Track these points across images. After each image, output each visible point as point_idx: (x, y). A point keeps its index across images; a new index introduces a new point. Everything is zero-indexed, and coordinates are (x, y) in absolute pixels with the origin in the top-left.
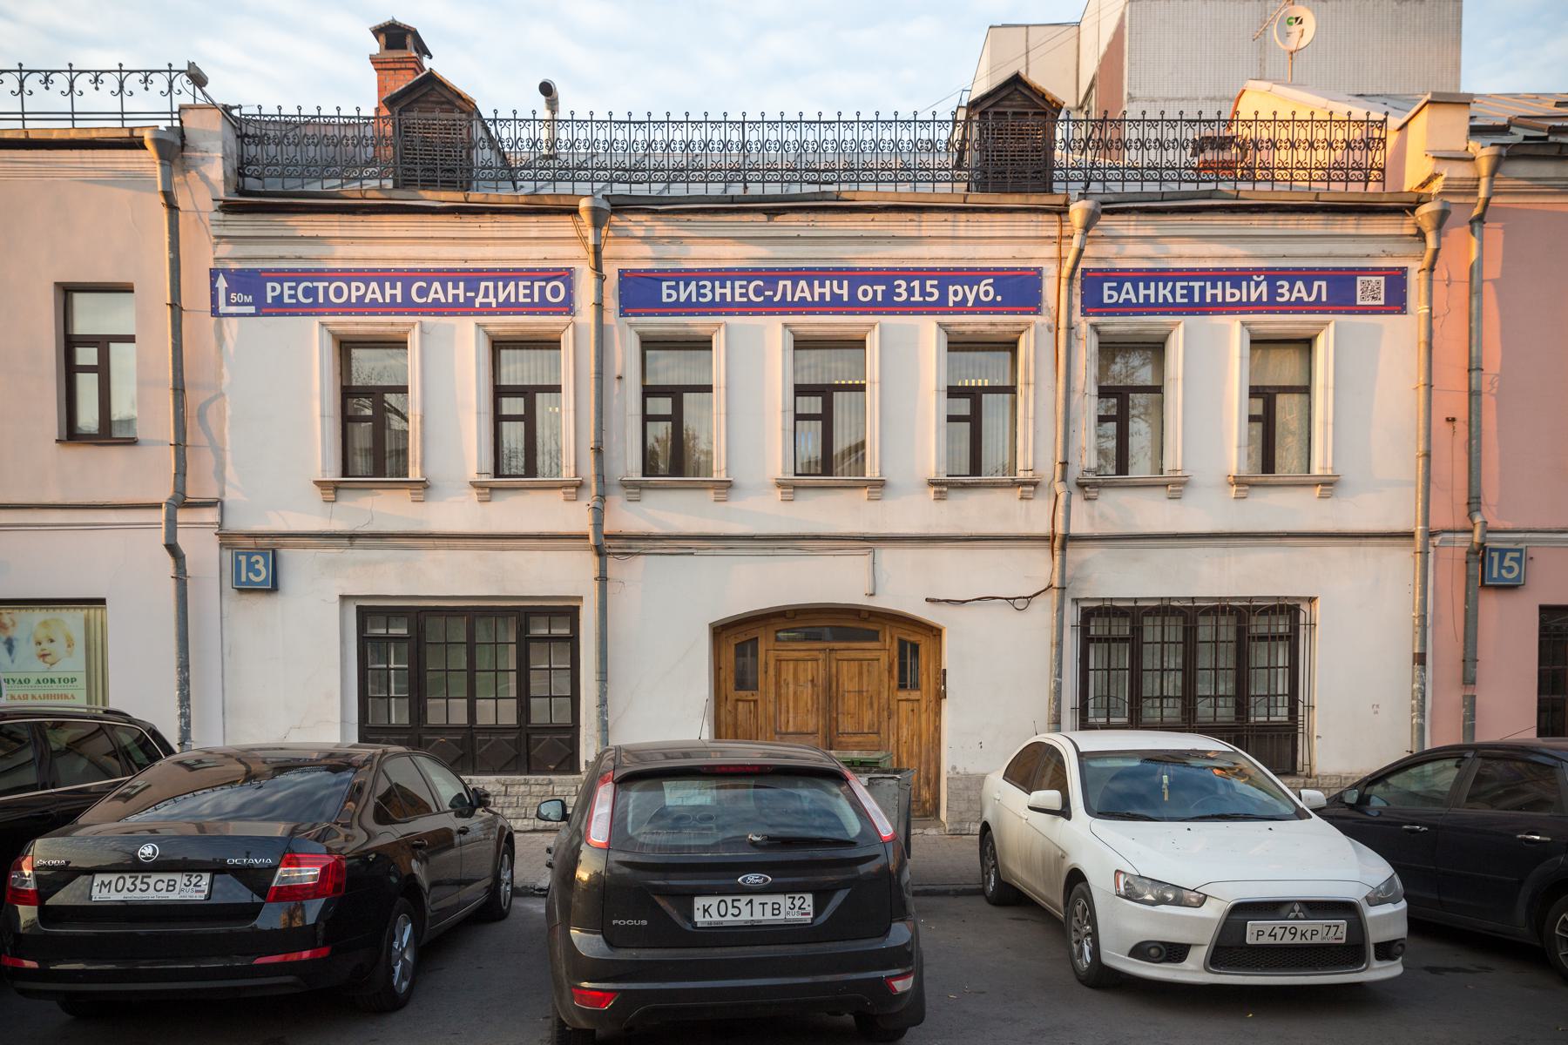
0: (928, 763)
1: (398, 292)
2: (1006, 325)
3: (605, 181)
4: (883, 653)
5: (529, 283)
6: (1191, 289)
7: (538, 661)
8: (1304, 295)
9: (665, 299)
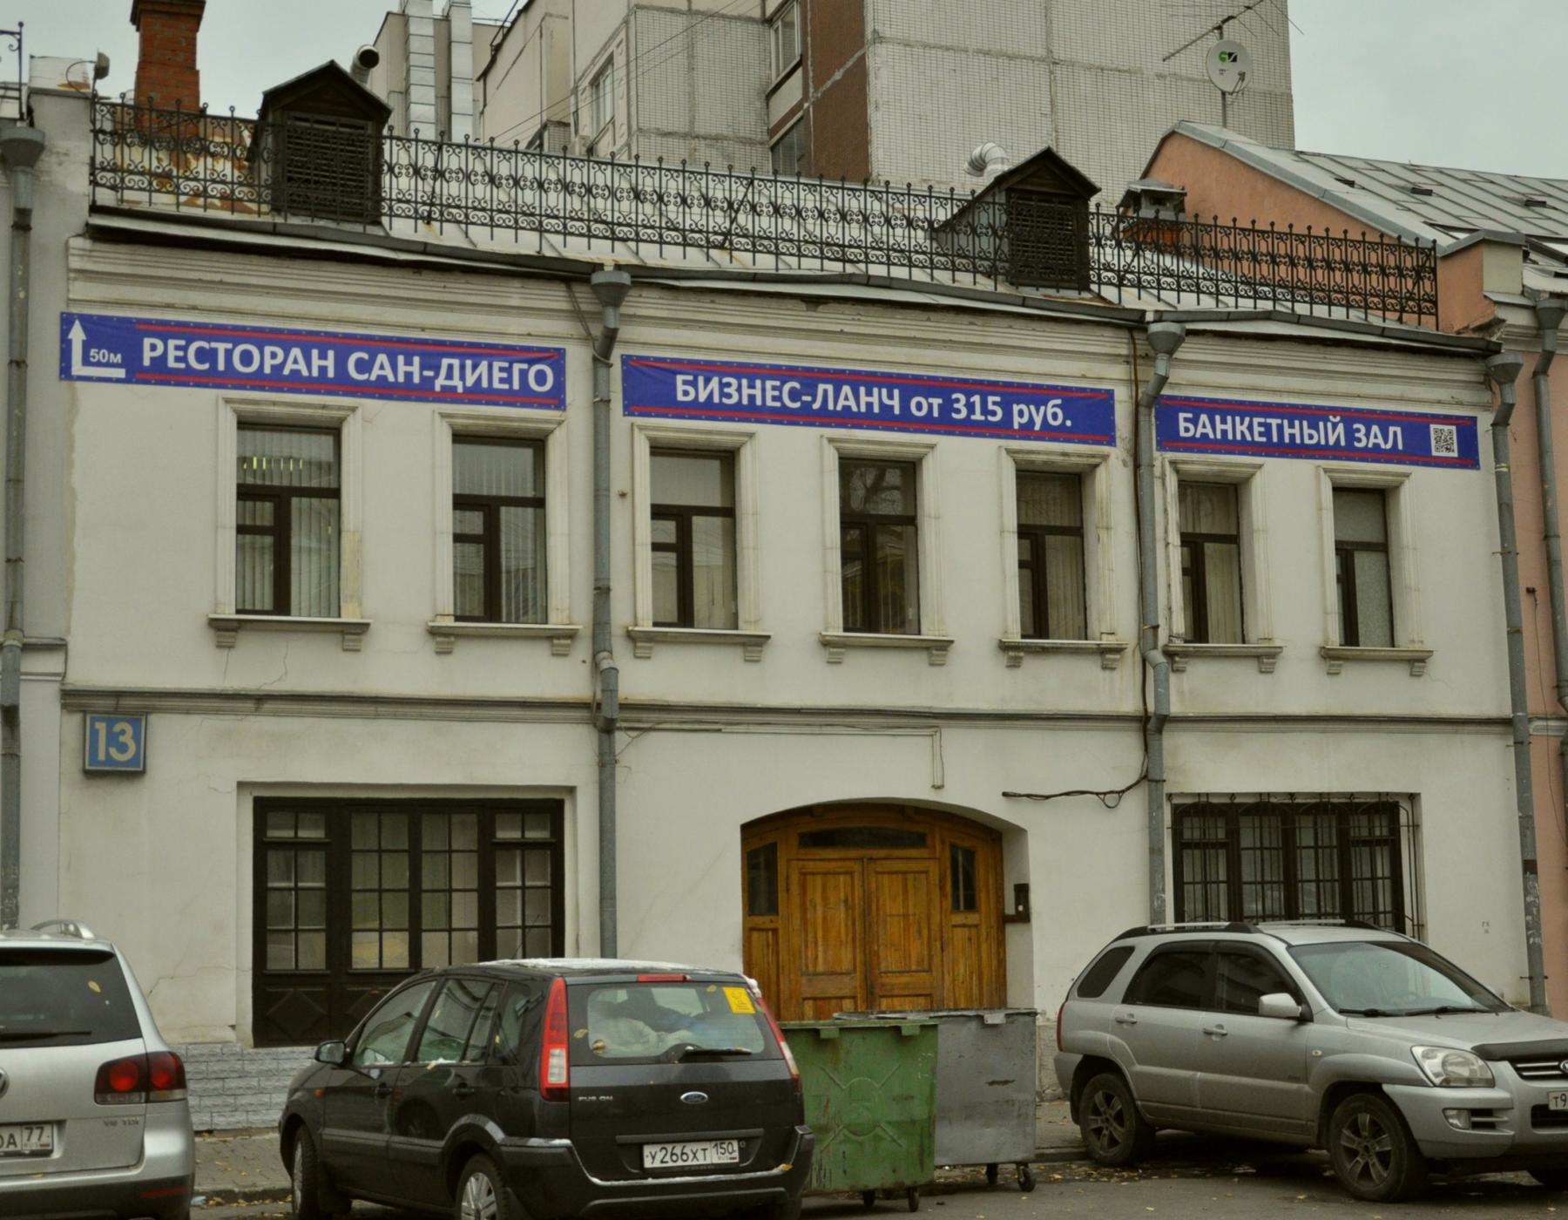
1: (330, 363)
2: (1080, 455)
6: (1268, 427)
8: (1380, 441)
9: (680, 397)
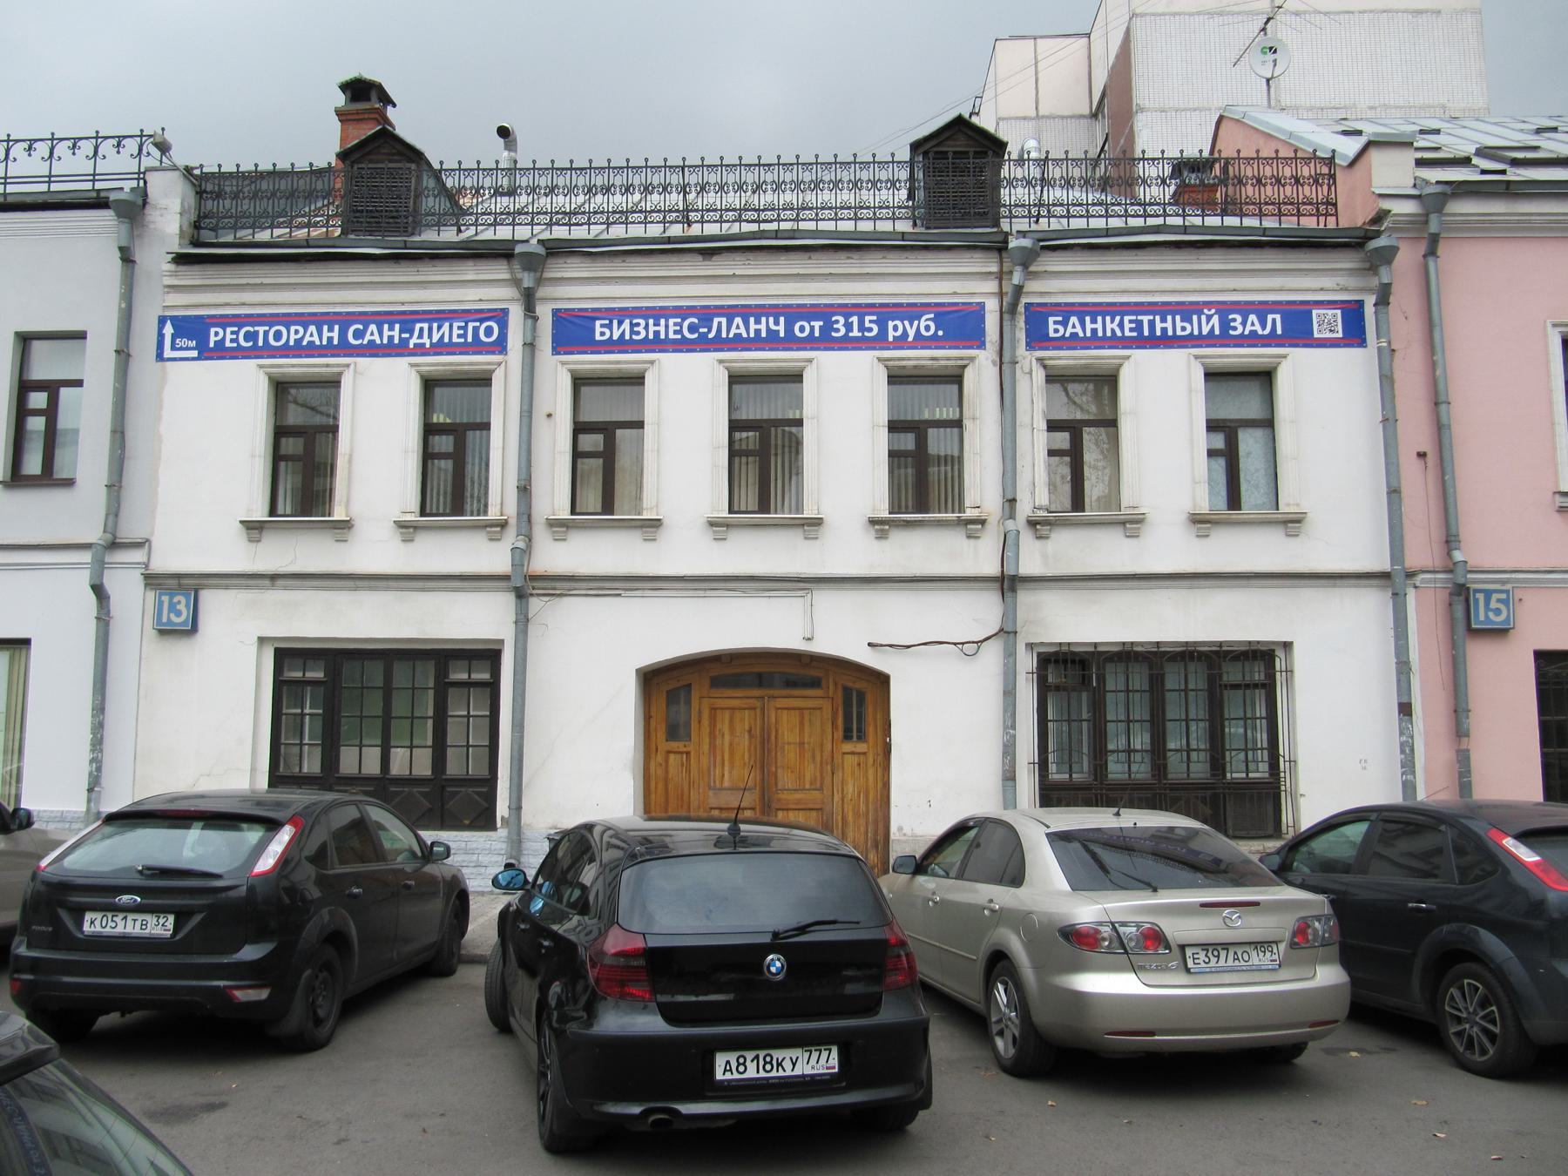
0: (876, 822)
1: (335, 335)
3: (545, 224)
5: (463, 324)
6: (1140, 323)
7: (456, 711)
8: (1258, 327)
9: (598, 337)
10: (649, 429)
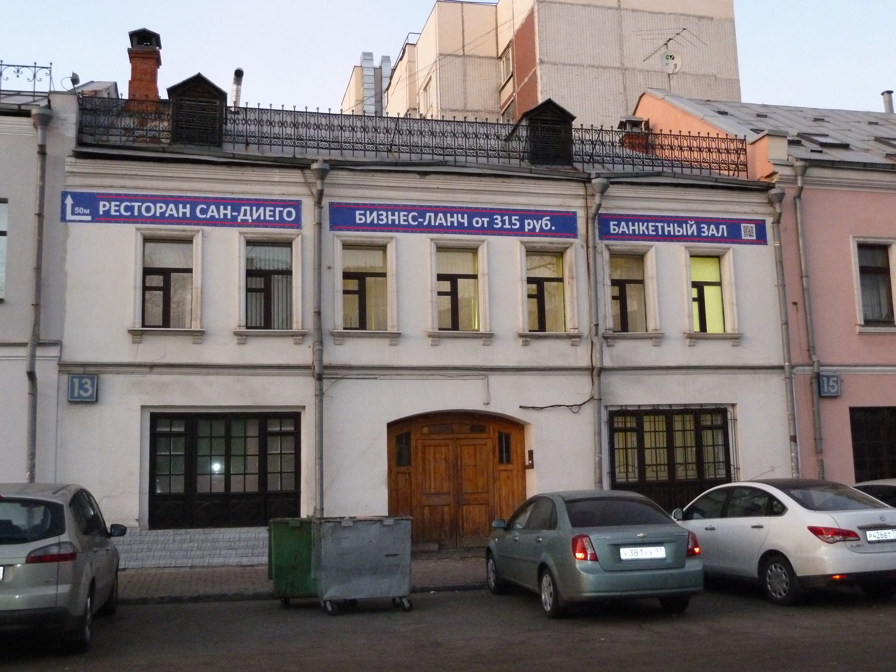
1: (188, 210)
2: (559, 243)
4: (489, 442)
6: (657, 227)
8: (715, 232)
10: (391, 280)
